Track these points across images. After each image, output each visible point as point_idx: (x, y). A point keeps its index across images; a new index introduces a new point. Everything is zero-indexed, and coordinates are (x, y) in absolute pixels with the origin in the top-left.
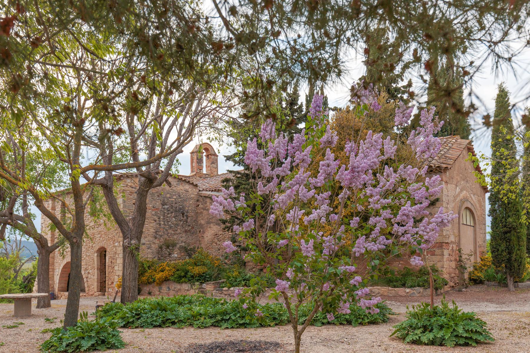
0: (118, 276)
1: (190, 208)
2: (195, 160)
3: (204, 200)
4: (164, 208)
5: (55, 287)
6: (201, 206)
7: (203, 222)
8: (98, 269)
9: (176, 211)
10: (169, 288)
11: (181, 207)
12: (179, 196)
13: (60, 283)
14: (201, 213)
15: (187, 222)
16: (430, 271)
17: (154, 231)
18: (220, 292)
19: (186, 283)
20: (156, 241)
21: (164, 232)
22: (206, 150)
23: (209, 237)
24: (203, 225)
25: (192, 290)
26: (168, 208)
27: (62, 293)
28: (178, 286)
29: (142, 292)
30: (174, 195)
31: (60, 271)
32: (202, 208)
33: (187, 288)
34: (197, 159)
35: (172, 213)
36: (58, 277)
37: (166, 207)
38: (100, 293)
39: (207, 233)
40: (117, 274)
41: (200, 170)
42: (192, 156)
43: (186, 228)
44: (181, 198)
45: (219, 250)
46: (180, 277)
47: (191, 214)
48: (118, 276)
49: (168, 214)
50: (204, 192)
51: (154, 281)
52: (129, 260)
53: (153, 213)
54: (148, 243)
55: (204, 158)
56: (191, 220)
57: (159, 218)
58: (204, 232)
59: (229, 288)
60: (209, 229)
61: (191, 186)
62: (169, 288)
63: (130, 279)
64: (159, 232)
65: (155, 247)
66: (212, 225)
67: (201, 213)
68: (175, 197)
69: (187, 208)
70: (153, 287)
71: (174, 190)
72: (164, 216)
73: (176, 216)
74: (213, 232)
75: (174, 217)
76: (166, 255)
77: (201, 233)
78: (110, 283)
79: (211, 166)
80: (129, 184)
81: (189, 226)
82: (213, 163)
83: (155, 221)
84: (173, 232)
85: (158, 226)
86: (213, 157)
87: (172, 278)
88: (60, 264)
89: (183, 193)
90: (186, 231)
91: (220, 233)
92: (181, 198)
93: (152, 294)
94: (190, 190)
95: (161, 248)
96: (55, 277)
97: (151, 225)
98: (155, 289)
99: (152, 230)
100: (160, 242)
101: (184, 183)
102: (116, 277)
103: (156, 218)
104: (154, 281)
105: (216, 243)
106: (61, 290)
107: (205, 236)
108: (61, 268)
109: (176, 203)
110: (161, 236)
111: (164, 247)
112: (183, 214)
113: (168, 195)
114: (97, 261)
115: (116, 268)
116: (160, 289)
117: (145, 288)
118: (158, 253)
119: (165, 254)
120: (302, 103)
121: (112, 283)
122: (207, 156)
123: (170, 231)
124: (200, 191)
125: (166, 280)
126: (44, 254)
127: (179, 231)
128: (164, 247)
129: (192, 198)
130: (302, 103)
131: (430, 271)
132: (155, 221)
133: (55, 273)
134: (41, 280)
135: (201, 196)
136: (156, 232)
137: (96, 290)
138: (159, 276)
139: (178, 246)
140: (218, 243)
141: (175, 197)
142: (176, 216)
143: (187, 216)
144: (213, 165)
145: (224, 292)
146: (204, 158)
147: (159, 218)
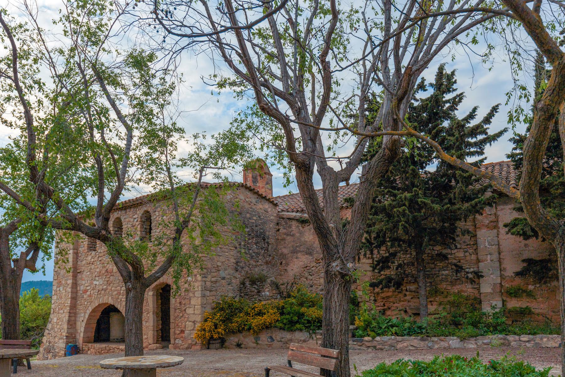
0: (194, 322)
1: (270, 233)
3: (286, 223)
5: (78, 337)
6: (282, 230)
7: (285, 251)
8: (153, 313)
9: (257, 236)
10: (271, 338)
11: (262, 231)
12: (259, 217)
13: (85, 332)
14: (283, 239)
15: (268, 251)
17: (234, 261)
18: (359, 344)
19: (301, 330)
20: (237, 275)
21: (245, 263)
24: (285, 255)
25: (311, 341)
26: (249, 232)
27: (90, 345)
28: (288, 336)
29: (226, 344)
31: (87, 316)
32: (285, 234)
33: (302, 339)
34: (253, 177)
35: (253, 238)
36: (84, 324)
38: (158, 345)
39: (292, 265)
40: (192, 318)
43: (267, 259)
44: (261, 219)
45: (311, 286)
46: (292, 323)
47: (272, 241)
48: (194, 322)
49: (249, 239)
50: (283, 213)
51: (249, 329)
52: (340, 296)
54: (228, 277)
57: (240, 245)
58: (287, 264)
59: (373, 338)
61: (271, 205)
62: (271, 338)
63: (341, 331)
64: (240, 262)
65: (236, 282)
66: (299, 255)
67: (283, 239)
68: (255, 218)
69: (267, 233)
70: (244, 337)
71: (254, 209)
75: (256, 244)
76: (253, 294)
77: (283, 265)
78: (178, 332)
79: (266, 186)
81: (270, 256)
82: (267, 183)
83: (236, 248)
84: (254, 264)
85: (238, 254)
86: (267, 176)
87: (279, 325)
88: (86, 308)
89: (262, 213)
90: (267, 263)
91: (312, 265)
92: (261, 219)
93: (242, 346)
94: (269, 210)
95: (243, 283)
96: (78, 324)
97: (232, 253)
98: (247, 340)
99: (233, 260)
100: (241, 276)
102: (189, 324)
104: (249, 329)
105: (306, 278)
106: (87, 341)
107: (289, 268)
108: (88, 312)
109: (256, 226)
110: (243, 268)
111: (247, 283)
112: (264, 240)
113: (248, 215)
114: (153, 302)
115: (190, 311)
116: (257, 339)
117: (232, 338)
118: (240, 290)
119: (251, 292)
120: (456, 90)
121: (182, 332)
123: (252, 262)
124: (279, 212)
125: (267, 327)
126: (138, 290)
127: (260, 262)
128: (247, 283)
129: (271, 221)
130: (456, 90)
132: (236, 248)
133: (77, 319)
134: (134, 331)
135: (283, 218)
136: (237, 263)
137: (151, 341)
138: (256, 322)
139: (269, 281)
140: (310, 277)
141: (255, 218)
143: (268, 243)
144: (268, 186)
145: (367, 343)
147: (240, 245)
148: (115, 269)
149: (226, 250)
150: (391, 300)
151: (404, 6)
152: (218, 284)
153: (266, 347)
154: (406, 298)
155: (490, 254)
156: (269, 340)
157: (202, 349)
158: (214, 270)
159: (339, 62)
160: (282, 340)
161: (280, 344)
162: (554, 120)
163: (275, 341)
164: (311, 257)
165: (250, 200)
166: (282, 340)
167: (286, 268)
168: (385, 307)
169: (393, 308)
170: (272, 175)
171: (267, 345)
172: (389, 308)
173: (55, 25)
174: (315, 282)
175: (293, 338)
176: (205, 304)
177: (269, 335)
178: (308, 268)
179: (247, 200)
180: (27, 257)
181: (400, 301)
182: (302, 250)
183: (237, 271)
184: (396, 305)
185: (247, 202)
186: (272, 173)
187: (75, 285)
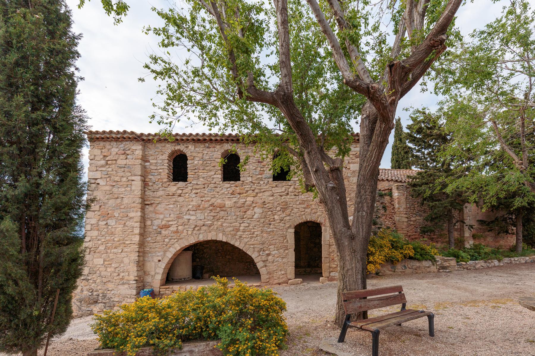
10: (405, 266)
33: (427, 265)
62: (405, 266)
88: (168, 246)
93: (380, 274)
151: (115, 149)
153: (400, 273)
155: (469, 216)
156: (403, 268)
159: (227, 147)
160: (413, 267)
161: (411, 270)
162: (66, 161)
163: (408, 269)
166: (413, 267)
171: (401, 272)
173: (185, 62)
175: (421, 265)
177: (403, 264)
180: (398, 295)
187: (143, 219)
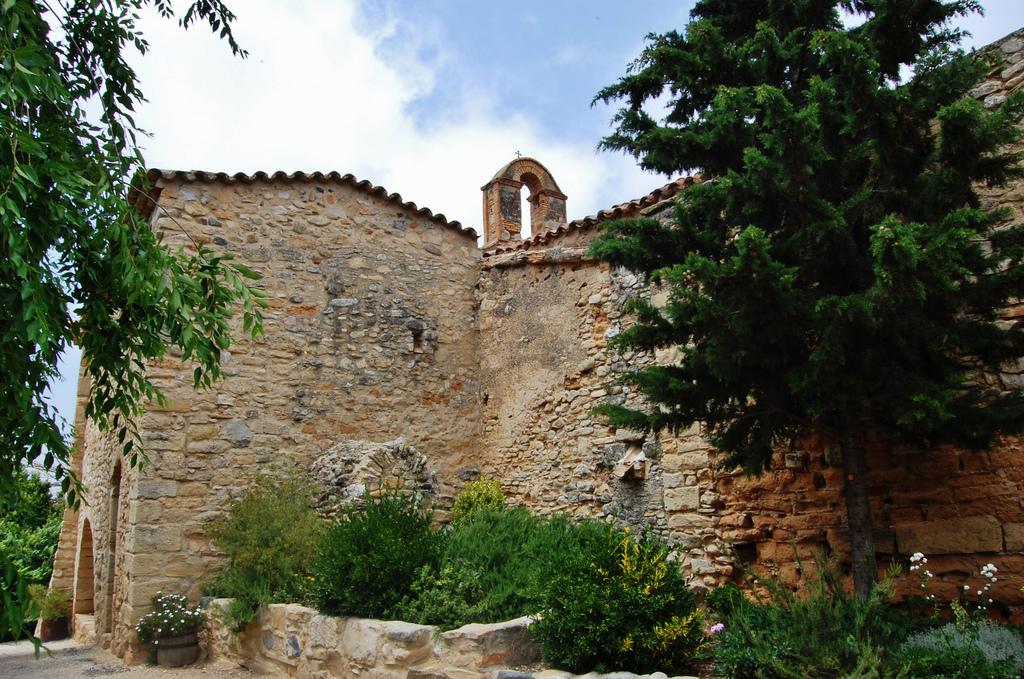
2: (495, 207)
4: (337, 308)
6: (488, 304)
7: (494, 363)
12: (404, 266)
15: (432, 362)
16: (63, 478)
17: (291, 392)
22: (529, 179)
23: (521, 418)
30: (380, 262)
35: (371, 324)
37: (343, 301)
41: (512, 233)
42: (486, 198)
43: (431, 387)
45: (556, 466)
49: (355, 328)
53: (291, 320)
54: (262, 438)
55: (526, 207)
56: (450, 356)
60: (517, 386)
61: (451, 235)
64: (311, 395)
66: (526, 368)
72: (337, 333)
73: (388, 338)
74: (531, 395)
75: (381, 343)
80: (190, 209)
81: (442, 378)
83: (299, 353)
84: (371, 398)
86: (551, 199)
94: (445, 248)
97: (282, 368)
101: (421, 226)
103: (301, 341)
105: (543, 440)
107: (503, 413)
113: (357, 262)
122: (534, 200)
131: (63, 478)
140: (553, 436)
141: (385, 269)
142: (388, 338)
146: (526, 207)
148: (996, 520)
149: (258, 360)
150: (772, 501)
152: (216, 460)
154: (823, 492)
157: (135, 661)
158: (204, 416)
164: (554, 374)
165: (372, 220)
167: (496, 413)
168: (754, 531)
169: (779, 533)
170: (564, 198)
172: (770, 535)
174: (565, 450)
176: (156, 521)
178: (548, 407)
179: (359, 219)
181: (803, 506)
182: (531, 353)
183: (298, 421)
184: (790, 519)
185: (358, 226)
186: (564, 191)
